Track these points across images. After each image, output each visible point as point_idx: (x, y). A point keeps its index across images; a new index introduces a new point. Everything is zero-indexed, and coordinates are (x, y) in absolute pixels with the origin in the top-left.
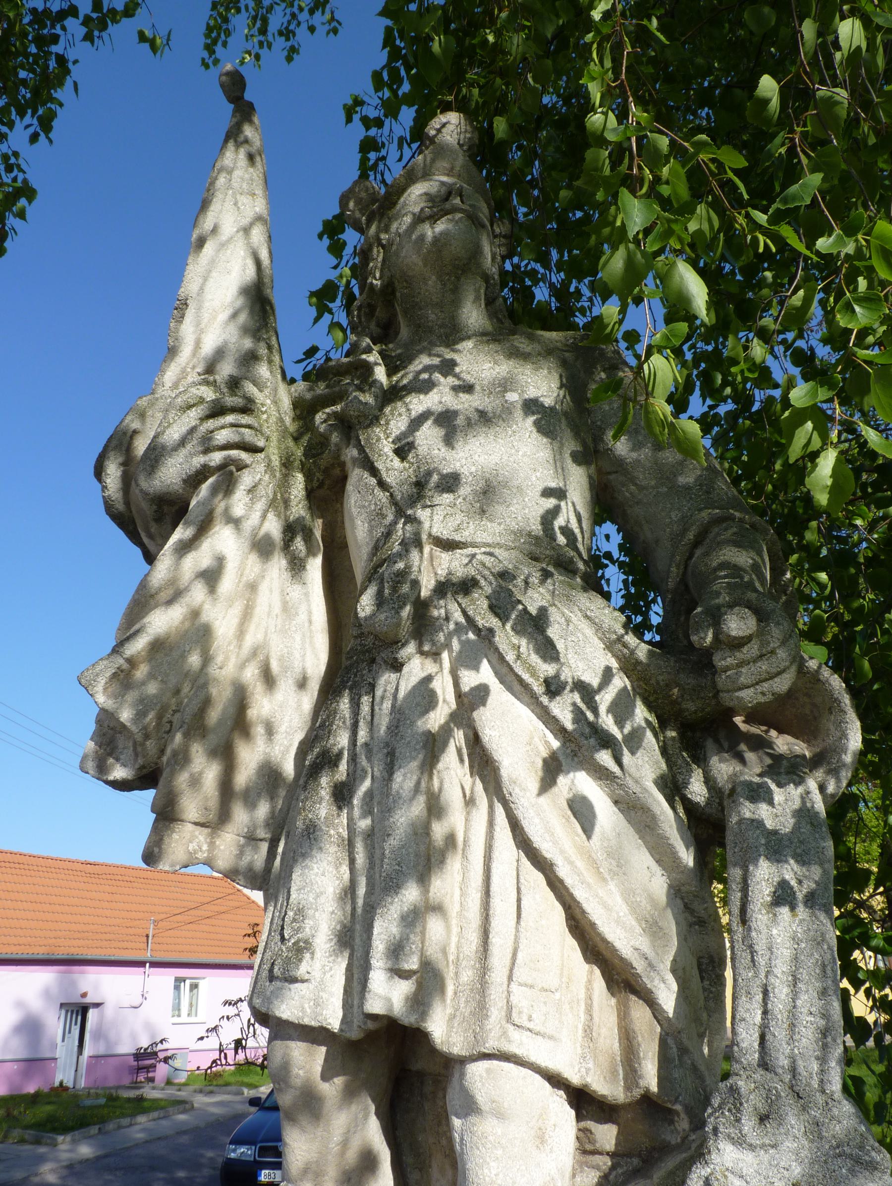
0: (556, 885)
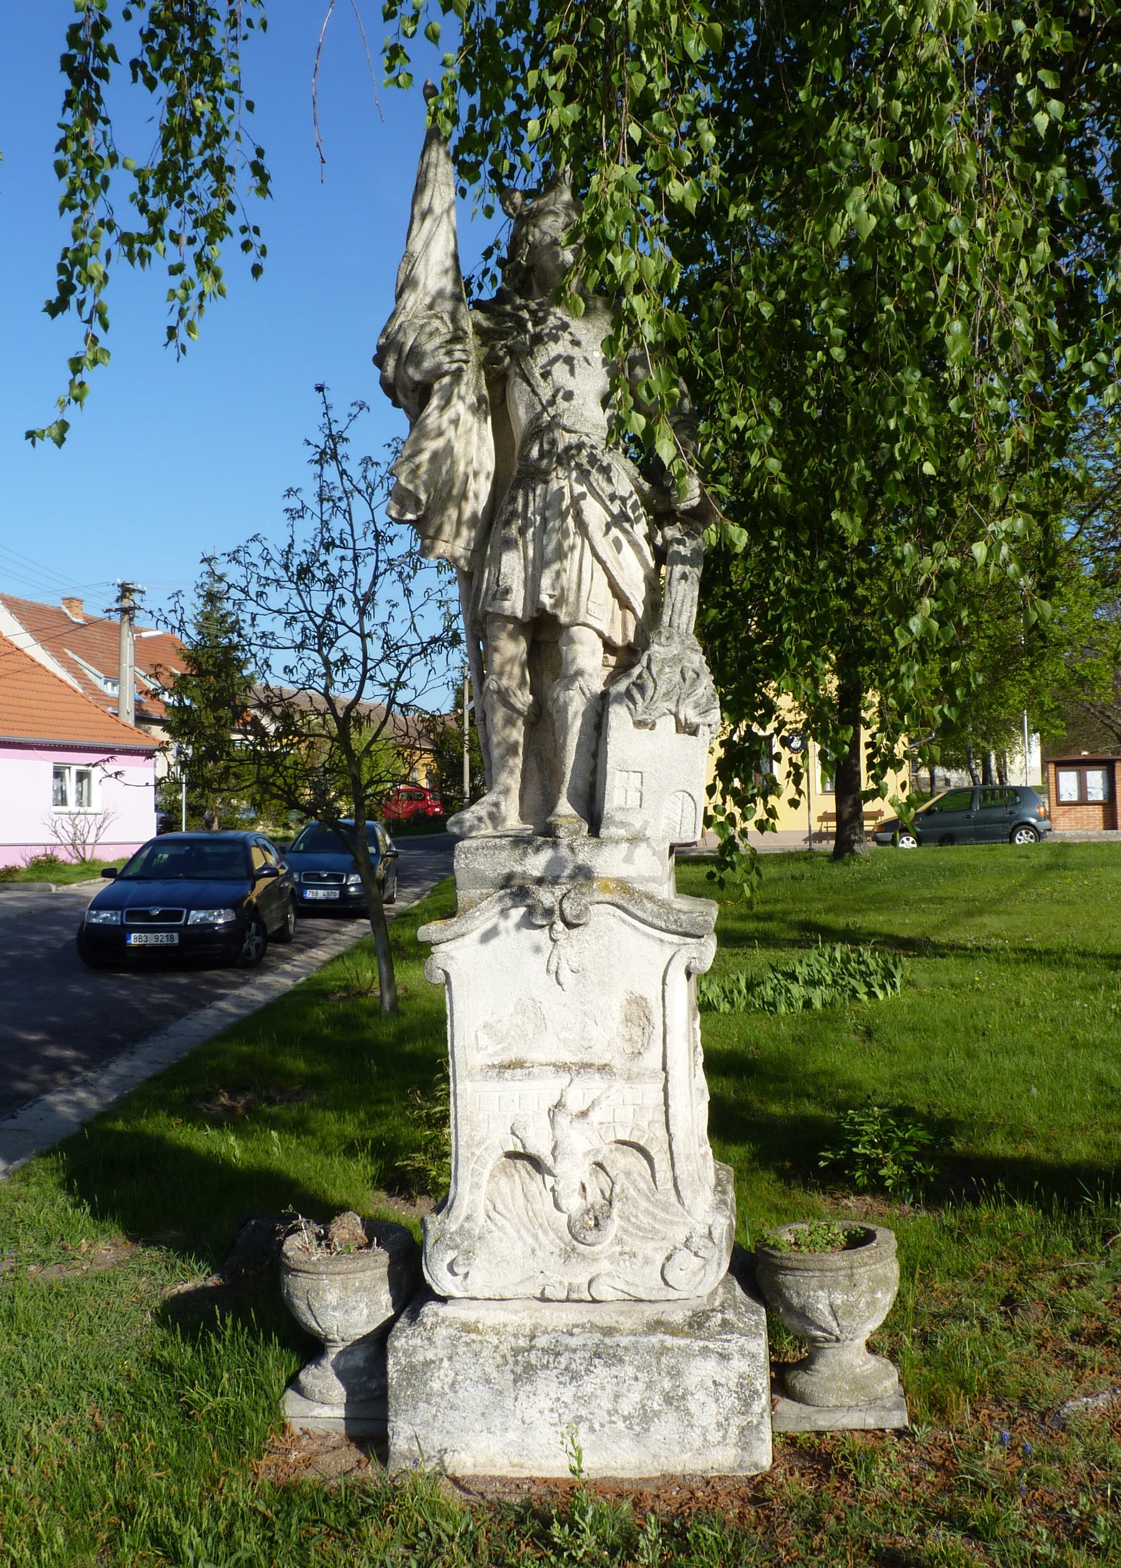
0: (606, 570)
